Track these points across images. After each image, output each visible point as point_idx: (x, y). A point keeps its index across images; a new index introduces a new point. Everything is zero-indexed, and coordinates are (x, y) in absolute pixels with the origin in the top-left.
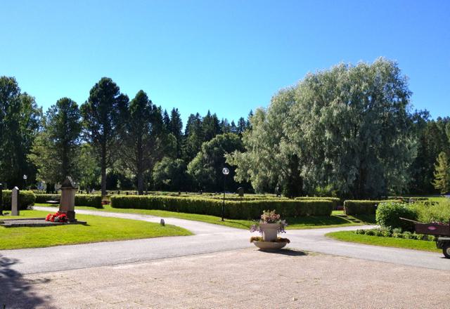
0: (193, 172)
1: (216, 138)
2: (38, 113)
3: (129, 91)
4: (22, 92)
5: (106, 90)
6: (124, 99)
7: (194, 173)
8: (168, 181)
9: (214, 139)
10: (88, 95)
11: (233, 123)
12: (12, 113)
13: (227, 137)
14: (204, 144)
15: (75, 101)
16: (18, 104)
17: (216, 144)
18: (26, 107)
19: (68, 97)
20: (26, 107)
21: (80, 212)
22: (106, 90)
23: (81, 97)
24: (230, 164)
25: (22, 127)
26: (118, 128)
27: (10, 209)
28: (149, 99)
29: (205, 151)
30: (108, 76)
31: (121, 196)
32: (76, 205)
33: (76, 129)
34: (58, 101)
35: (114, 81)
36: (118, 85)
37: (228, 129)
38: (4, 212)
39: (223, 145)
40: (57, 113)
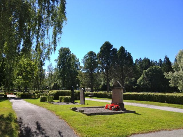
0: (140, 83)
1: (150, 68)
2: (77, 61)
3: (117, 46)
4: (72, 53)
5: (107, 47)
6: (115, 50)
7: (140, 84)
8: (136, 87)
9: (149, 69)
10: (100, 50)
11: (156, 62)
12: (68, 61)
13: (155, 67)
14: (144, 71)
15: (95, 52)
16: (71, 58)
17: (150, 71)
18: (73, 59)
19: (92, 51)
20: (73, 59)
21: (128, 104)
22: (107, 47)
23: (97, 51)
24: (167, 78)
25: (72, 67)
26: (113, 63)
27: (79, 99)
28: (125, 50)
29: (144, 74)
30: (108, 41)
31: (134, 94)
32: (124, 99)
33: (96, 64)
34: (88, 53)
35: (110, 43)
36: (112, 44)
37: (154, 64)
38: (75, 101)
39: (154, 71)
40: (88, 58)
